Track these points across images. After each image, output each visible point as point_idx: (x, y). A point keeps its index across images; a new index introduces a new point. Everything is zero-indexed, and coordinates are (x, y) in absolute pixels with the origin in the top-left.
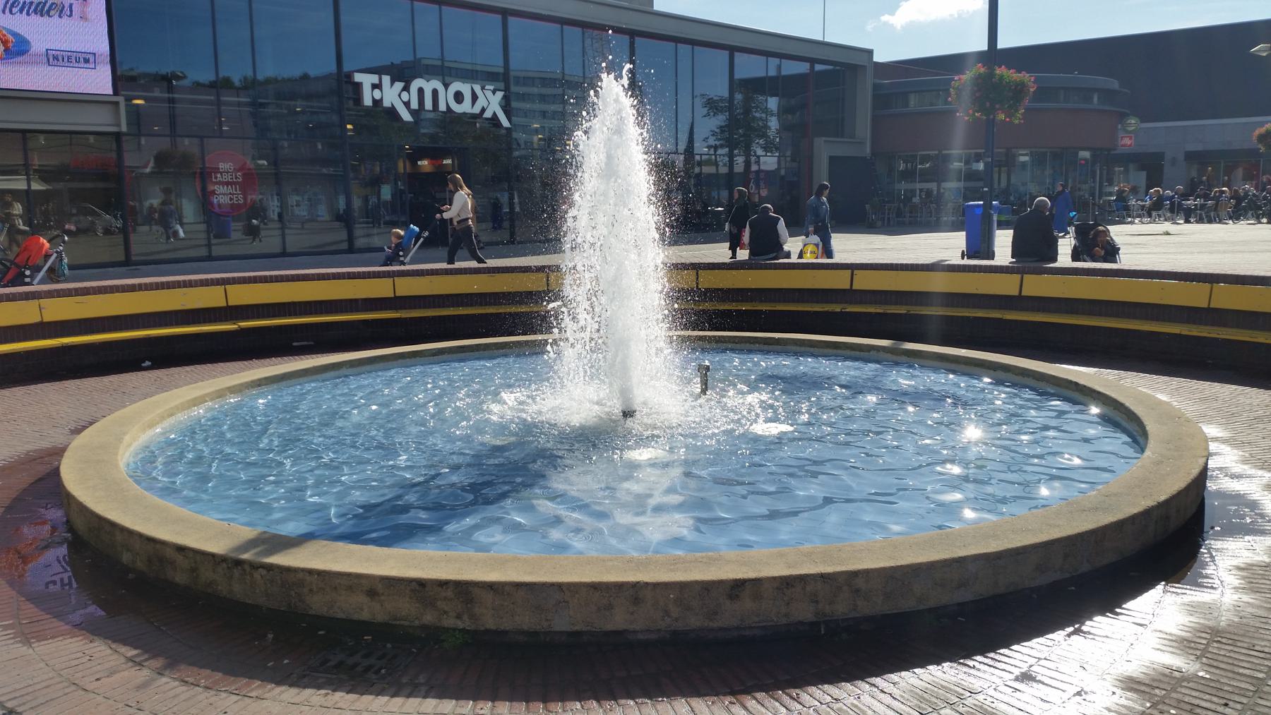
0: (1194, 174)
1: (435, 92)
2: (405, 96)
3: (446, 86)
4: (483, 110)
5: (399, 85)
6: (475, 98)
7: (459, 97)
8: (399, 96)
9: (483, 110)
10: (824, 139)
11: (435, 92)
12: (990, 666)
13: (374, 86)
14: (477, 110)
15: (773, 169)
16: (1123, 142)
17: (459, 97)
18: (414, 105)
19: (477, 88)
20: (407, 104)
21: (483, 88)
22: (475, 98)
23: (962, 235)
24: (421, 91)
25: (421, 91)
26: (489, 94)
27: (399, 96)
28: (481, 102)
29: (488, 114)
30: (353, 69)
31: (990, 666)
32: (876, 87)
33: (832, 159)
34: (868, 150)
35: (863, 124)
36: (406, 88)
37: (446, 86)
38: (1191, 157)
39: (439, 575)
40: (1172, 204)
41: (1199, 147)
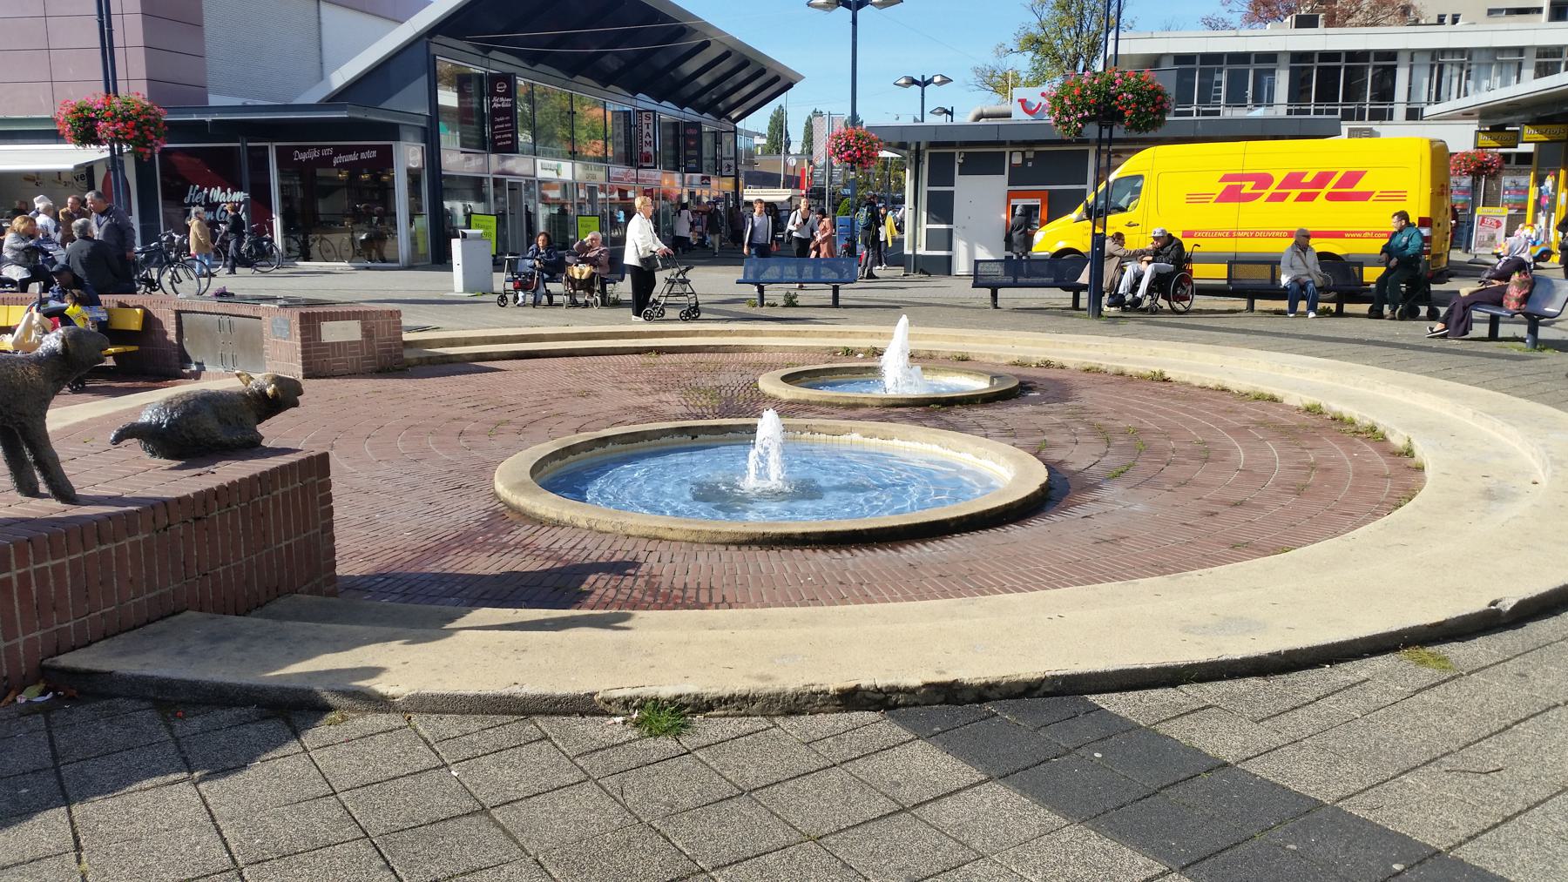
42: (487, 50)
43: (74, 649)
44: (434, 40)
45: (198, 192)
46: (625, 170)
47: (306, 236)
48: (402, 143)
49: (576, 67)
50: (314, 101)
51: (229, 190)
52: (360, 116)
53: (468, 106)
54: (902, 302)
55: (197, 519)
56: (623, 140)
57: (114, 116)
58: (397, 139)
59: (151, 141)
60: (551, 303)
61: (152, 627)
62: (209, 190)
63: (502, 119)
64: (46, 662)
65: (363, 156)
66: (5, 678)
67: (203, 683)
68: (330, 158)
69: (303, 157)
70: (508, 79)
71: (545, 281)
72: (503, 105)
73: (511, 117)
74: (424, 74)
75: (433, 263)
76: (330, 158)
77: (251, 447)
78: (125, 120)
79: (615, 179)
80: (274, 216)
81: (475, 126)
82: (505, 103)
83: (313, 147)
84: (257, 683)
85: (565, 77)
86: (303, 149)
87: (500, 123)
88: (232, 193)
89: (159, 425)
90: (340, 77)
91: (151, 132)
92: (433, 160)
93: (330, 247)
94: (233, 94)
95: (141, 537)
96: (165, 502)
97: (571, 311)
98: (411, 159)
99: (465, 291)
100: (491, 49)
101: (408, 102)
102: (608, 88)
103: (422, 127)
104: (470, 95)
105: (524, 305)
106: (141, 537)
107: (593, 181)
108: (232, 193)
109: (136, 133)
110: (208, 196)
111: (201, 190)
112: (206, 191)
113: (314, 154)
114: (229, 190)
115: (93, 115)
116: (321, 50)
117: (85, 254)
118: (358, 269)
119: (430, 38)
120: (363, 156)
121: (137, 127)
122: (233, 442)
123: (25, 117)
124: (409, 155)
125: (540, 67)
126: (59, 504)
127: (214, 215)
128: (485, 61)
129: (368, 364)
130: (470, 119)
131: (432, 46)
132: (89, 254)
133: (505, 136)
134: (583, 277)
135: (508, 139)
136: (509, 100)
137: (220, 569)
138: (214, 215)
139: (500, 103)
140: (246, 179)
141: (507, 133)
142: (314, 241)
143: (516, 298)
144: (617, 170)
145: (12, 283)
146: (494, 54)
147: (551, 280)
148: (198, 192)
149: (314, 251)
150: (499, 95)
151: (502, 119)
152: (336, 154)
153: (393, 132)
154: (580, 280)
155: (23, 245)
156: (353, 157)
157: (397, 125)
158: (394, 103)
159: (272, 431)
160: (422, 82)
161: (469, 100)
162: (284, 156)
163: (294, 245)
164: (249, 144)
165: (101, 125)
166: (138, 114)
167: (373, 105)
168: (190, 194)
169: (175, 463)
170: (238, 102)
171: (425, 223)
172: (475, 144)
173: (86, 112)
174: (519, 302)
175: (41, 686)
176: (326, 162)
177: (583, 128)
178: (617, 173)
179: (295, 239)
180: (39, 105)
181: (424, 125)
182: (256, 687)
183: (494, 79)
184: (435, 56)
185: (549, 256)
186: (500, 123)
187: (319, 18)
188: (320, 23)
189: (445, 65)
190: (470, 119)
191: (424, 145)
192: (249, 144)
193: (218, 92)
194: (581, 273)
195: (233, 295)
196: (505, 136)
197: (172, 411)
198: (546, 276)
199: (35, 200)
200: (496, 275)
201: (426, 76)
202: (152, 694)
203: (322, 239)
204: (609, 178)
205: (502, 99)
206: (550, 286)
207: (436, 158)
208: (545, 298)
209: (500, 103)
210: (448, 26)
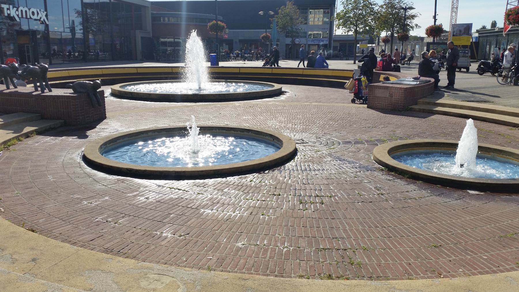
0: (241, 46)
1: (26, 11)
2: (17, 13)
3: (29, 9)
4: (41, 18)
5: (15, 9)
6: (38, 14)
7: (33, 13)
8: (15, 12)
9: (41, 18)
10: (139, 31)
11: (26, 11)
12: (467, 79)
13: (8, 9)
14: (39, 18)
15: (454, 86)
16: (225, 36)
17: (33, 13)
18: (20, 16)
19: (38, 11)
20: (18, 15)
21: (40, 10)
22: (38, 14)
23: (439, 85)
24: (22, 11)
25: (22, 11)
26: (42, 12)
27: (15, 12)
28: (40, 15)
29: (42, 20)
30: (48, 12)
31: (467, 79)
32: (152, 14)
33: (142, 37)
34: (151, 36)
35: (149, 28)
36: (17, 10)
37: (29, 9)
38: (241, 41)
39: (152, 126)
40: (242, 56)
41: (243, 38)
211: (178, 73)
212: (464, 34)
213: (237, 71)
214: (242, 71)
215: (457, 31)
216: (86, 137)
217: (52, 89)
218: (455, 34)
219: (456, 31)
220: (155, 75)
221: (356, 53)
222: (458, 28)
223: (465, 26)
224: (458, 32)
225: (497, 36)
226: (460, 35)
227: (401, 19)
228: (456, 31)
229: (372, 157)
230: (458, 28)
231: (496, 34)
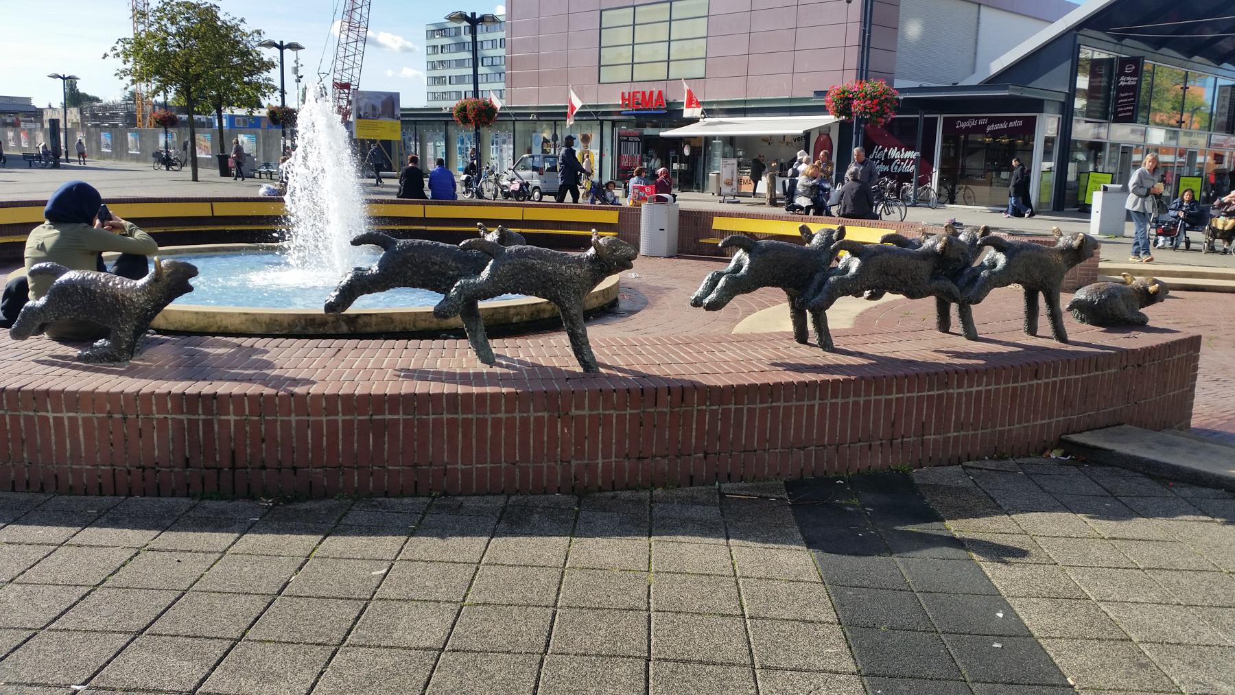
42: (1120, 39)
43: (1081, 432)
44: (1081, 32)
45: (880, 151)
46: (1225, 137)
47: (954, 186)
48: (1044, 115)
49: (1191, 49)
50: (975, 83)
51: (903, 150)
52: (1018, 94)
53: (1098, 84)
54: (75, 367)
55: (1139, 365)
56: (1227, 111)
57: (865, 97)
58: (1041, 111)
59: (886, 114)
60: (1188, 248)
61: (1110, 429)
62: (889, 150)
63: (1126, 94)
64: (1063, 437)
65: (1011, 125)
66: (1045, 441)
67: (1183, 468)
68: (985, 126)
69: (963, 125)
70: (1137, 62)
71: (1186, 229)
72: (1129, 83)
73: (1135, 93)
74: (1068, 59)
75: (1054, 210)
76: (985, 126)
77: (1141, 324)
78: (872, 99)
79: (1216, 145)
80: (934, 170)
81: (1101, 101)
82: (1131, 81)
83: (972, 118)
84: (1227, 475)
85: (1185, 58)
86: (964, 120)
87: (1124, 98)
88: (905, 152)
89: (1092, 302)
90: (996, 66)
91: (888, 107)
92: (1065, 132)
93: (972, 194)
94: (909, 79)
95: (1113, 371)
96: (1127, 351)
97: (1210, 256)
98: (1049, 127)
99: (1100, 234)
100: (1124, 37)
101: (1051, 84)
102: (1221, 66)
103: (1061, 102)
104: (1100, 76)
105: (1163, 248)
106: (1113, 371)
107: (1194, 147)
108: (905, 152)
109: (878, 108)
110: (887, 153)
111: (883, 149)
112: (886, 150)
113: (973, 123)
114: (903, 150)
115: (851, 96)
116: (976, 43)
117: (854, 191)
118: (994, 212)
119: (1078, 31)
120: (1011, 125)
121: (880, 104)
122: (1133, 319)
123: (757, 98)
124: (1048, 125)
125: (1164, 50)
126: (1058, 342)
127: (890, 168)
128: (1118, 47)
129: (1070, 283)
130: (1098, 95)
131: (1079, 37)
132: (857, 191)
133: (1127, 108)
134: (1227, 228)
135: (1129, 111)
136: (1135, 79)
137: (1142, 402)
138: (890, 168)
139: (1127, 81)
140: (919, 143)
141: (1128, 106)
142: (960, 189)
143: (1156, 242)
144: (1219, 137)
145: (801, 208)
146: (1127, 42)
147: (1191, 229)
148: (880, 151)
149: (959, 196)
150: (1127, 75)
151: (1126, 94)
152: (990, 123)
153: (1038, 106)
154: (1223, 230)
155: (810, 183)
156: (1003, 126)
157: (1042, 101)
158: (1039, 83)
159: (1153, 313)
160: (1066, 66)
161: (1099, 79)
162: (948, 124)
163: (944, 191)
164: (926, 116)
165: (855, 102)
166: (881, 95)
167: (1023, 84)
168: (874, 152)
169: (1101, 329)
170: (916, 85)
171: (1052, 178)
172: (1098, 115)
173: (846, 94)
174: (1159, 245)
175: (1062, 451)
176: (980, 129)
177: (1168, 101)
178: (1219, 140)
179: (946, 188)
180: (804, 90)
181: (1063, 100)
182: (1226, 477)
183: (1124, 62)
184: (1079, 45)
185: (1192, 209)
186: (1124, 98)
187: (979, 18)
188: (978, 23)
189: (1086, 53)
190: (1098, 95)
191: (1061, 116)
192: (926, 116)
193: (901, 78)
194: (1225, 225)
195: (961, 224)
196: (1127, 108)
197: (1101, 294)
198: (1187, 225)
199: (798, 153)
200: (1128, 224)
201: (1070, 60)
202: (1141, 468)
203: (966, 188)
204: (1209, 144)
205: (1129, 78)
206: (1189, 234)
207: (1068, 127)
208: (1183, 245)
209: (1127, 81)
210: (1096, 22)
211: (276, 217)
212: (383, 114)
213: (203, 210)
214: (221, 210)
215: (365, 106)
216: (190, 289)
217: (798, 233)
218: (362, 113)
219: (363, 108)
220: (417, 225)
221: (128, 149)
222: (367, 100)
223: (384, 98)
224: (370, 111)
225: (446, 123)
226: (375, 117)
227: (162, 44)
228: (363, 108)
229: (98, 455)
230: (367, 100)
231: (445, 119)
